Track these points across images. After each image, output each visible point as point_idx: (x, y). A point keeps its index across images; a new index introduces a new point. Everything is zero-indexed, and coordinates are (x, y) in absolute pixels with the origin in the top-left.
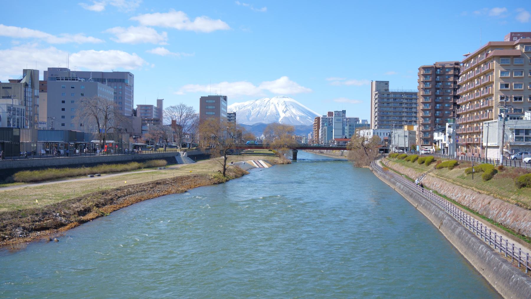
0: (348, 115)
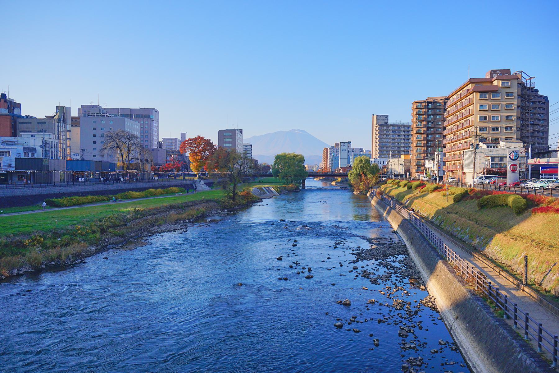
0: (353, 146)
